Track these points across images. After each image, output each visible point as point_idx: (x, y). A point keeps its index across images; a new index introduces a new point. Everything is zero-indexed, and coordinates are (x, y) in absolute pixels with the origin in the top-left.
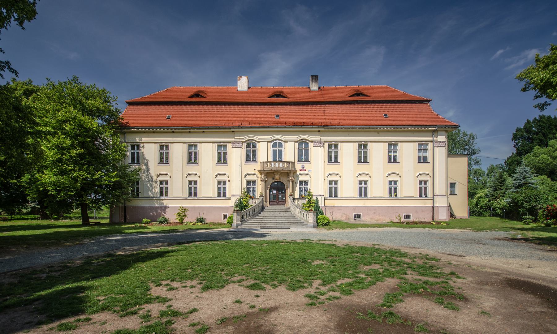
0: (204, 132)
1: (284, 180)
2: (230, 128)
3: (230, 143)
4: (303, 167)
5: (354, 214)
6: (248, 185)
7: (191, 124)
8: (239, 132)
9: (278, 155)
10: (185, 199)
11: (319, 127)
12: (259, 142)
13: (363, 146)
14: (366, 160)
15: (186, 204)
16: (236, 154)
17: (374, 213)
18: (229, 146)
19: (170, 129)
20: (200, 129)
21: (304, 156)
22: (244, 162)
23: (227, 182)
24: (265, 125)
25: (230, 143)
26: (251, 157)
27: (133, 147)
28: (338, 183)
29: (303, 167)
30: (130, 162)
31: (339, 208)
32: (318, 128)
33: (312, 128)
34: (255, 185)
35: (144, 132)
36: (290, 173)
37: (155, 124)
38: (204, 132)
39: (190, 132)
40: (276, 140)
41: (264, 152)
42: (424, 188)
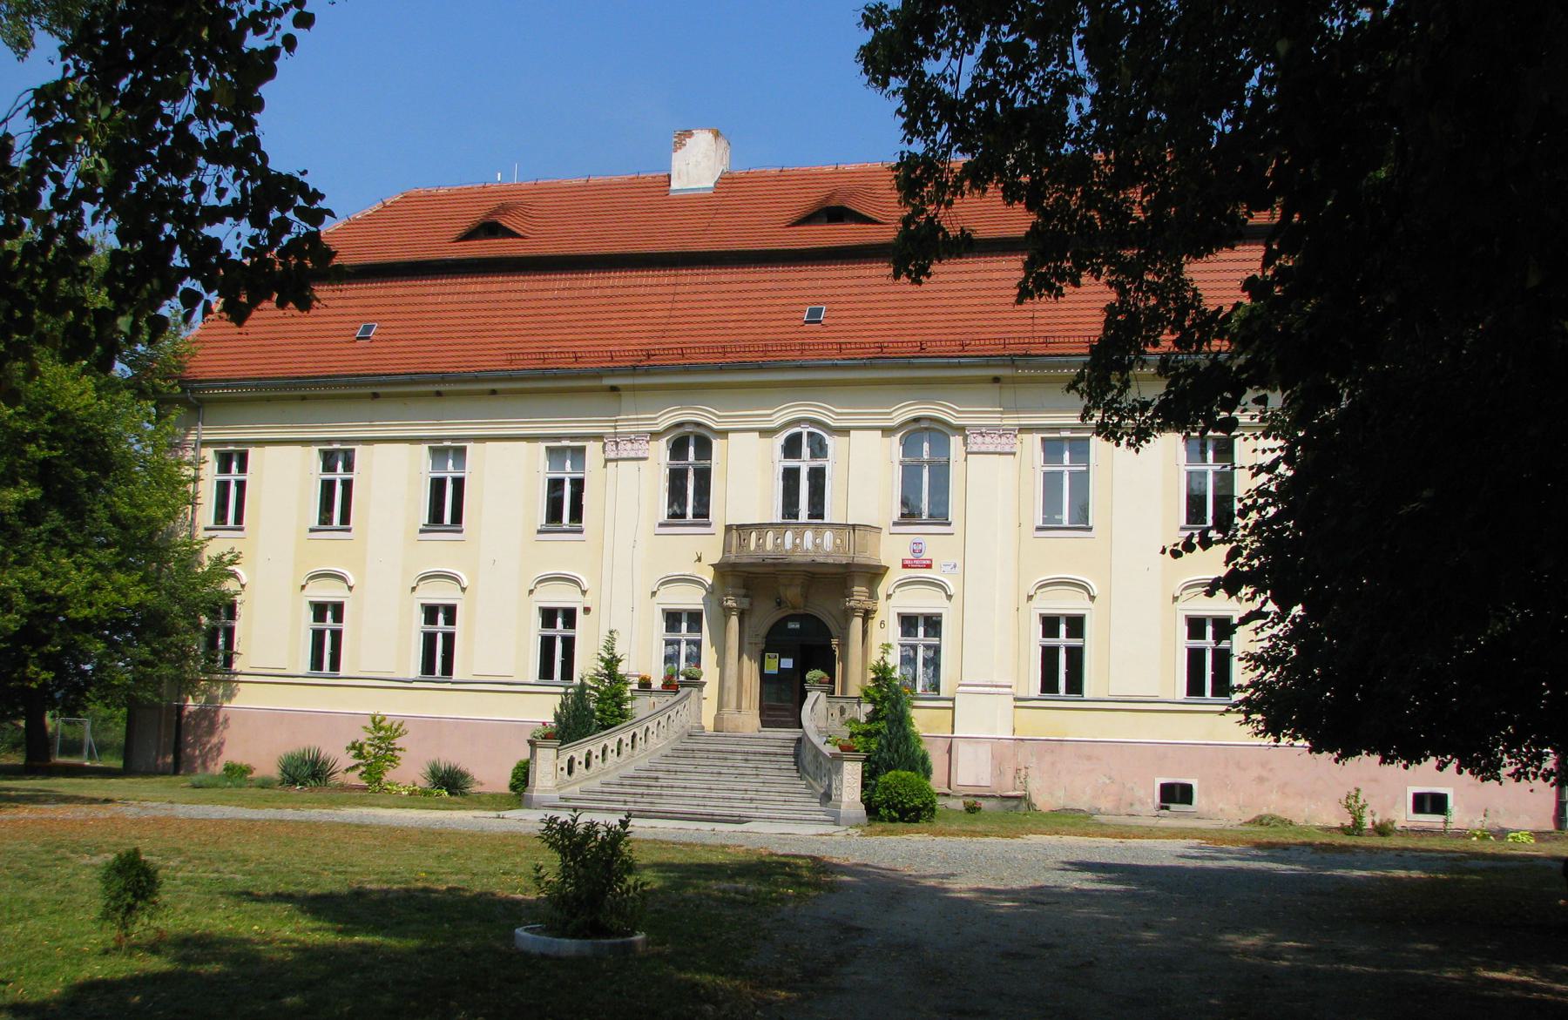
0: (494, 392)
1: (822, 608)
2: (598, 375)
3: (598, 437)
4: (917, 549)
5: (1159, 781)
6: (905, 633)
7: (444, 362)
8: (634, 389)
9: (804, 491)
10: (405, 684)
11: (988, 360)
12: (723, 434)
13: (449, 451)
14: (1081, 520)
15: (394, 706)
16: (629, 485)
17: (1261, 779)
18: (593, 449)
19: (366, 385)
20: (476, 380)
21: (927, 499)
22: (1029, 529)
23: (580, 615)
24: (748, 357)
25: (598, 437)
26: (688, 493)
27: (224, 463)
28: (1089, 627)
29: (917, 549)
30: (211, 523)
31: (1087, 750)
32: (988, 366)
33: (960, 366)
34: (938, 634)
35: (269, 399)
36: (844, 581)
37: (309, 368)
38: (494, 392)
39: (439, 394)
40: (797, 422)
41: (747, 477)
42: (1069, 650)
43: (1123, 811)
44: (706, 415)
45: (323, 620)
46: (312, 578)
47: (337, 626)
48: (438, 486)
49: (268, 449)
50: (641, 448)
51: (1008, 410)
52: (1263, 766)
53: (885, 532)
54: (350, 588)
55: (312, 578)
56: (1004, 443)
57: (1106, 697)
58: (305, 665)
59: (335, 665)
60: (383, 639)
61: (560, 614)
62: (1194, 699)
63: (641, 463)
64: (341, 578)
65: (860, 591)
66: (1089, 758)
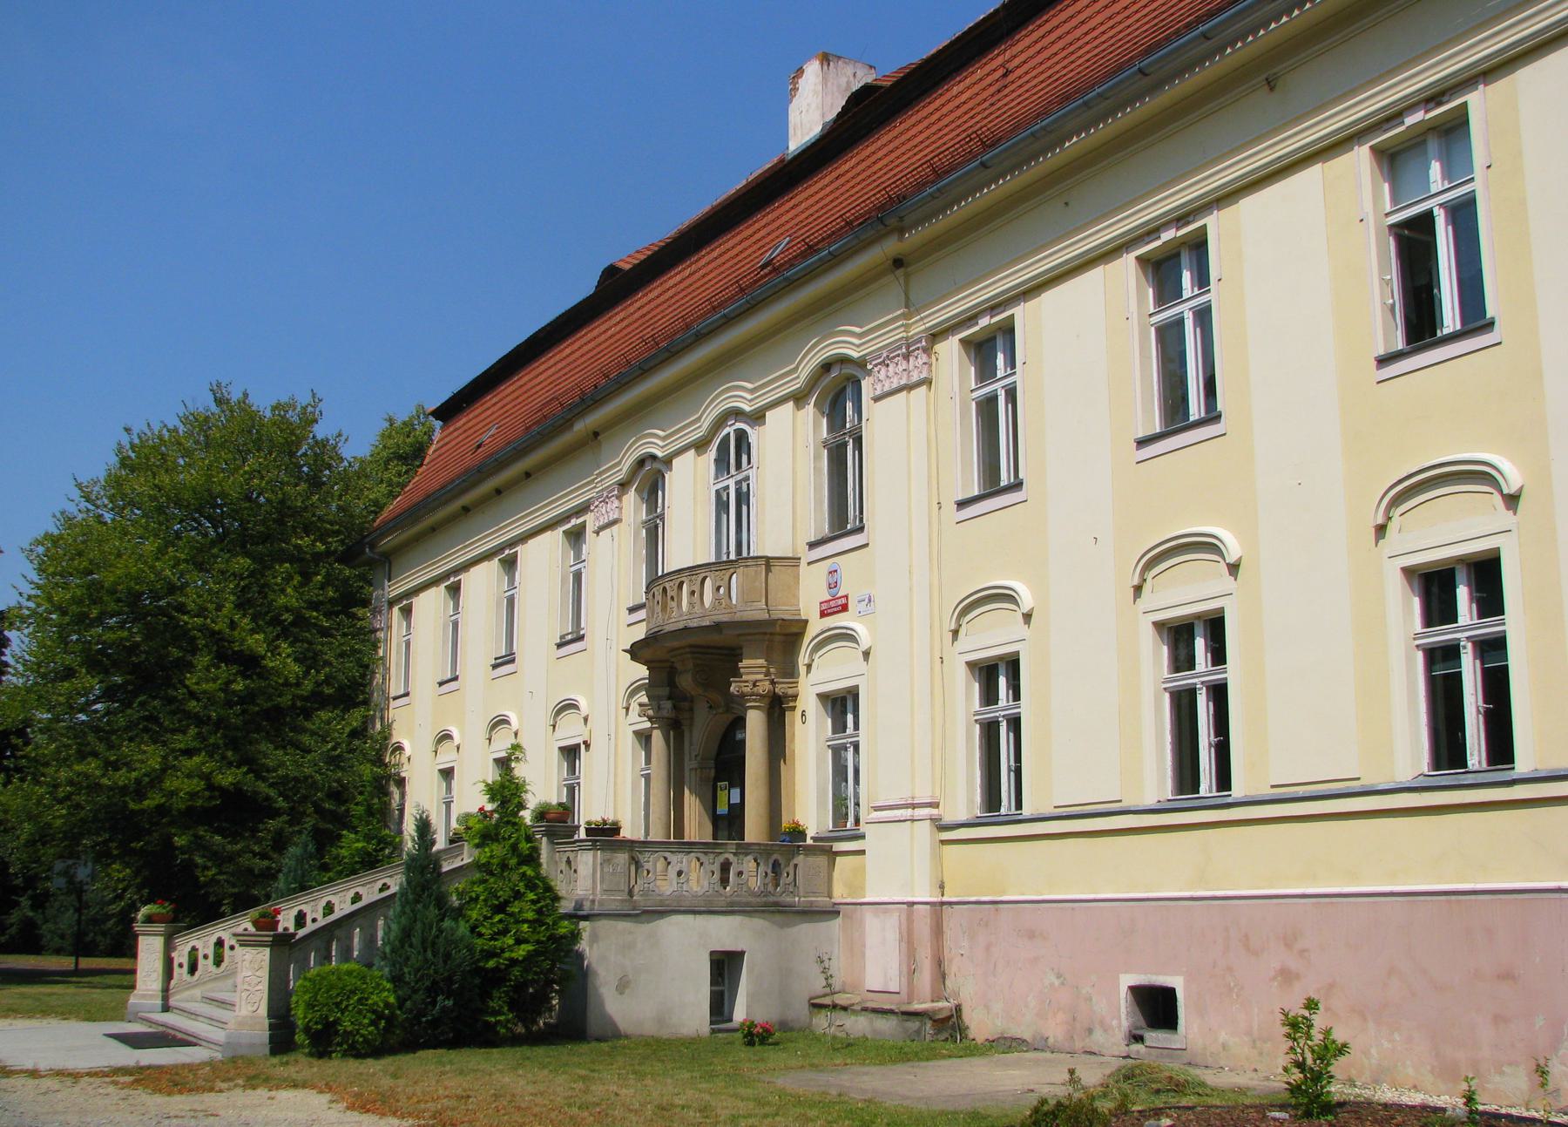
5: (1129, 979)
39: (466, 510)
43: (1078, 1045)
44: (847, 343)
45: (1190, 664)
46: (1150, 565)
47: (1489, 628)
48: (1413, 242)
49: (1247, 204)
50: (608, 511)
51: (912, 307)
52: (1288, 941)
53: (803, 563)
54: (1512, 500)
55: (1150, 565)
56: (916, 367)
57: (1267, 792)
58: (1157, 782)
59: (1501, 748)
60: (1099, 726)
61: (1461, 576)
62: (1448, 776)
63: (615, 528)
64: (1479, 476)
65: (753, 672)
66: (1031, 935)
